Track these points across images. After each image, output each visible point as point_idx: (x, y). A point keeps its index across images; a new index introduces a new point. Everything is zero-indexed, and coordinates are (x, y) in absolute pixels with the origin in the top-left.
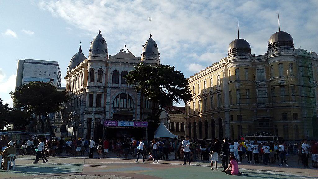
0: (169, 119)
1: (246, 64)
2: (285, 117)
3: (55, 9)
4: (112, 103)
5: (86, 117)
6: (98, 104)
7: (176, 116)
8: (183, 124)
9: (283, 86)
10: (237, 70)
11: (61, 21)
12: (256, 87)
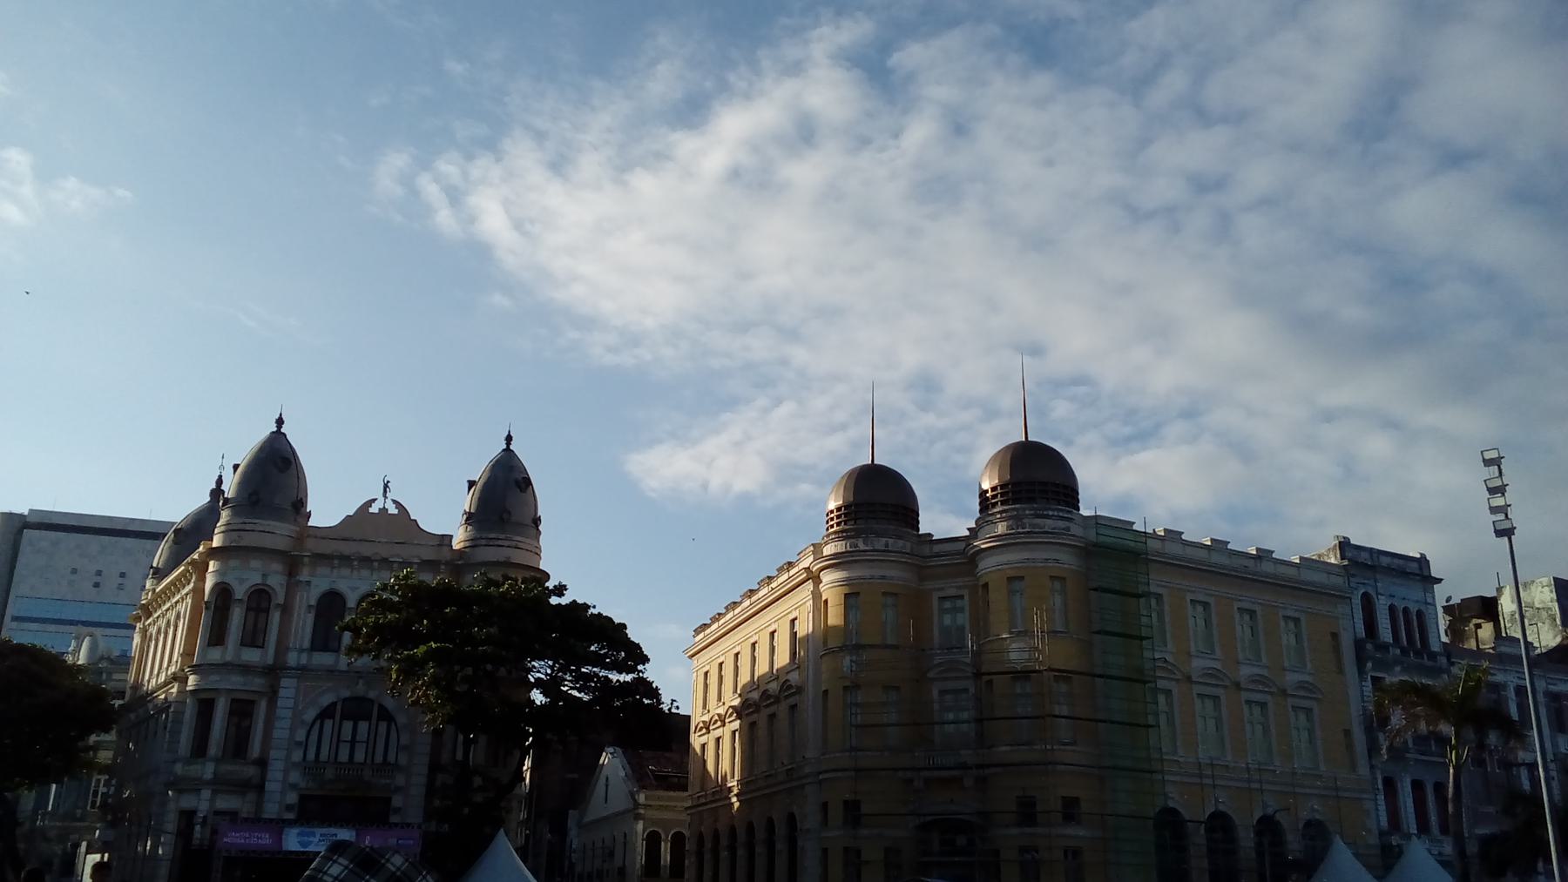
0: (638, 817)
1: (888, 573)
2: (1028, 812)
3: (455, 197)
4: (299, 744)
5: (172, 806)
6: (237, 746)
7: (670, 799)
8: (678, 840)
9: (1024, 675)
10: (852, 600)
11: (473, 262)
12: (931, 675)
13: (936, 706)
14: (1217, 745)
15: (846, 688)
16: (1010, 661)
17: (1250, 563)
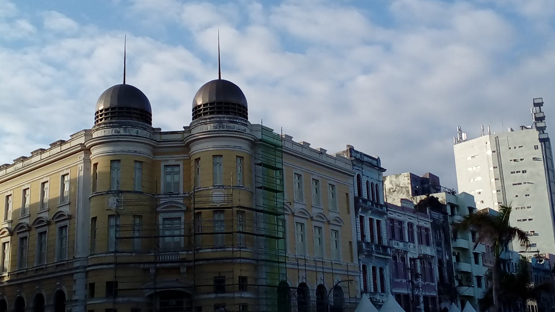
2: (220, 285)
9: (219, 210)
13: (161, 227)
14: (317, 248)
15: (110, 216)
16: (212, 202)
17: (317, 156)
